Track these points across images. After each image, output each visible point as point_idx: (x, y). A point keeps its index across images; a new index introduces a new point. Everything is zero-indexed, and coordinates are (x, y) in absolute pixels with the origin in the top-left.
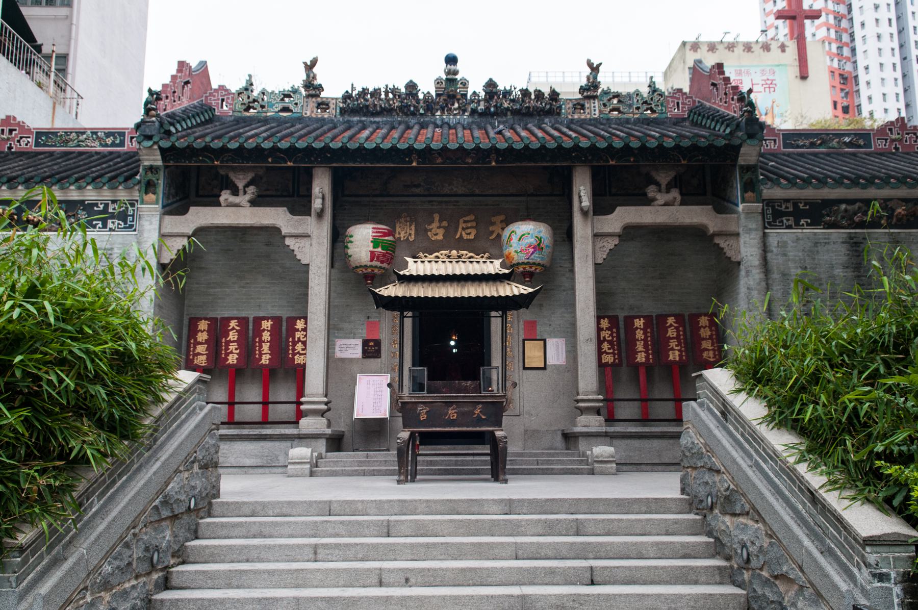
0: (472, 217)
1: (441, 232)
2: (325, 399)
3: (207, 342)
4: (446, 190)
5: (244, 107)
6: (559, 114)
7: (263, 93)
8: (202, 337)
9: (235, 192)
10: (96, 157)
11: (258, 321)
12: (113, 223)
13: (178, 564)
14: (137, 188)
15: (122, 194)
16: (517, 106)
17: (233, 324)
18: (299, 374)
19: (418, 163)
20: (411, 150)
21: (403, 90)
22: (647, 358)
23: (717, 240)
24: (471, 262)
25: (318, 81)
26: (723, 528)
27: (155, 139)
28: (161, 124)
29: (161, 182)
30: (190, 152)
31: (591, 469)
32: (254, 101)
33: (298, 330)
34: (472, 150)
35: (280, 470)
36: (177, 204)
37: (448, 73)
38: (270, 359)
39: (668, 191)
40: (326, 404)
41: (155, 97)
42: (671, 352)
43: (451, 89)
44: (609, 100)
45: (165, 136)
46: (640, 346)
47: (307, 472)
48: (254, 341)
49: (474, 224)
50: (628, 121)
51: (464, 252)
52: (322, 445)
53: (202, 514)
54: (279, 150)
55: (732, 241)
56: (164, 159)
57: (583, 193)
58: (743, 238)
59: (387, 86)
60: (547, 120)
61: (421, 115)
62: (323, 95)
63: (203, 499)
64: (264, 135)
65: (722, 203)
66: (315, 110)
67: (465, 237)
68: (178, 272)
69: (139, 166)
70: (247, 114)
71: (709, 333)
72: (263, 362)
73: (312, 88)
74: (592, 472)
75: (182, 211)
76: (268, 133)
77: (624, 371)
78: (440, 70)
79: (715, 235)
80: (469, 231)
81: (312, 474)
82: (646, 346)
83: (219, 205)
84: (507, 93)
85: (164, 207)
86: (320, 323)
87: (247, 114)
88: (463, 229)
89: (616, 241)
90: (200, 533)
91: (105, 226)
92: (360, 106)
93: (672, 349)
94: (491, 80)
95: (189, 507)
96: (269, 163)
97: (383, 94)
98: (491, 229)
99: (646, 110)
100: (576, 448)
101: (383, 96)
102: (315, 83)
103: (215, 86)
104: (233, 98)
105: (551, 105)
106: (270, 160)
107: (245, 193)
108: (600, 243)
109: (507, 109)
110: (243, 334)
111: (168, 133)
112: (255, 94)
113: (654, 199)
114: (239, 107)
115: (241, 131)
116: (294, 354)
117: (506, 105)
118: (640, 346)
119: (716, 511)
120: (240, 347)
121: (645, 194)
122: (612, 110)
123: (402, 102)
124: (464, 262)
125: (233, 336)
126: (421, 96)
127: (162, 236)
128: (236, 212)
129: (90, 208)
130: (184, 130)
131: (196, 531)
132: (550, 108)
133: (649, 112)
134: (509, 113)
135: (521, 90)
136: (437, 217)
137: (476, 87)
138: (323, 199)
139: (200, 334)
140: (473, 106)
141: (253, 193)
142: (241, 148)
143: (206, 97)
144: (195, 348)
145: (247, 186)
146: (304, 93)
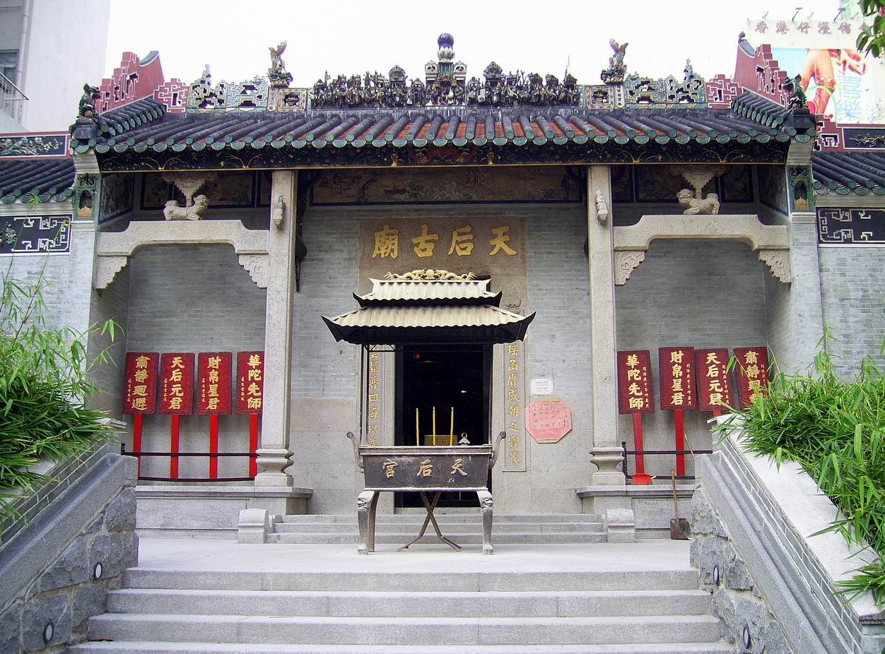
0: (468, 229)
1: (430, 247)
2: (286, 452)
3: (146, 382)
4: (437, 197)
5: (200, 102)
6: (576, 104)
7: (222, 86)
8: (141, 376)
9: (182, 202)
10: (32, 166)
11: (204, 358)
12: (44, 242)
13: (81, 642)
14: (70, 201)
15: (55, 209)
16: (525, 94)
17: (177, 361)
18: (255, 421)
19: (399, 163)
20: (389, 148)
21: (387, 77)
22: (685, 399)
23: (763, 256)
24: (450, 283)
25: (287, 69)
26: (727, 606)
27: (92, 143)
28: (99, 126)
29: (98, 193)
30: (130, 158)
31: (604, 538)
32: (212, 95)
33: (251, 368)
34: (464, 147)
35: (233, 533)
36: (116, 219)
37: (442, 56)
38: (218, 404)
39: (704, 197)
40: (287, 456)
41: (92, 93)
42: (712, 396)
43: (445, 79)
44: (637, 87)
45: (104, 140)
46: (677, 385)
47: (262, 537)
48: (200, 380)
49: (471, 237)
50: (659, 113)
51: (443, 272)
52: (282, 505)
53: (114, 585)
54: (174, 154)
55: (780, 257)
56: (101, 166)
57: (600, 194)
58: (795, 254)
59: (368, 74)
60: (562, 111)
61: (409, 106)
62: (292, 85)
63: (113, 566)
64: (216, 134)
65: (768, 212)
66: (282, 103)
67: (460, 253)
68: (116, 299)
69: (74, 176)
70: (202, 111)
71: (757, 372)
72: (210, 407)
73: (280, 78)
74: (605, 539)
75: (122, 227)
76: (221, 132)
77: (660, 415)
78: (432, 54)
79: (758, 251)
80: (463, 245)
81: (266, 540)
82: (684, 385)
83: (163, 219)
84: (512, 80)
85: (100, 222)
86: (279, 360)
87: (202, 111)
88: (457, 243)
89: (642, 257)
90: (109, 606)
91: (35, 246)
92: (337, 96)
93: (714, 391)
94: (493, 63)
95: (94, 575)
96: (658, 161)
97: (363, 82)
98: (492, 242)
99: (683, 98)
100: (591, 510)
101: (363, 85)
102: (283, 72)
103: (167, 79)
104: (187, 94)
105: (567, 92)
106: (222, 164)
107: (193, 203)
108: (622, 259)
109: (514, 98)
110: (187, 373)
111: (107, 136)
112: (213, 86)
113: (687, 207)
114: (193, 102)
115: (191, 130)
116: (247, 397)
117: (511, 94)
118: (677, 385)
119: (722, 586)
120: (184, 389)
121: (677, 201)
122: (640, 100)
123: (385, 92)
124: (442, 283)
125: (176, 376)
126: (408, 84)
127: (98, 257)
128: (182, 225)
129: (16, 224)
130: (131, 129)
131: (105, 604)
132: (566, 96)
133: (686, 101)
134: (515, 103)
135: (530, 76)
136: (425, 229)
137: (475, 71)
138: (284, 208)
139: (138, 373)
140: (472, 94)
141: (202, 204)
142: (188, 151)
143: (156, 93)
144: (133, 389)
145: (195, 195)
146: (269, 84)
